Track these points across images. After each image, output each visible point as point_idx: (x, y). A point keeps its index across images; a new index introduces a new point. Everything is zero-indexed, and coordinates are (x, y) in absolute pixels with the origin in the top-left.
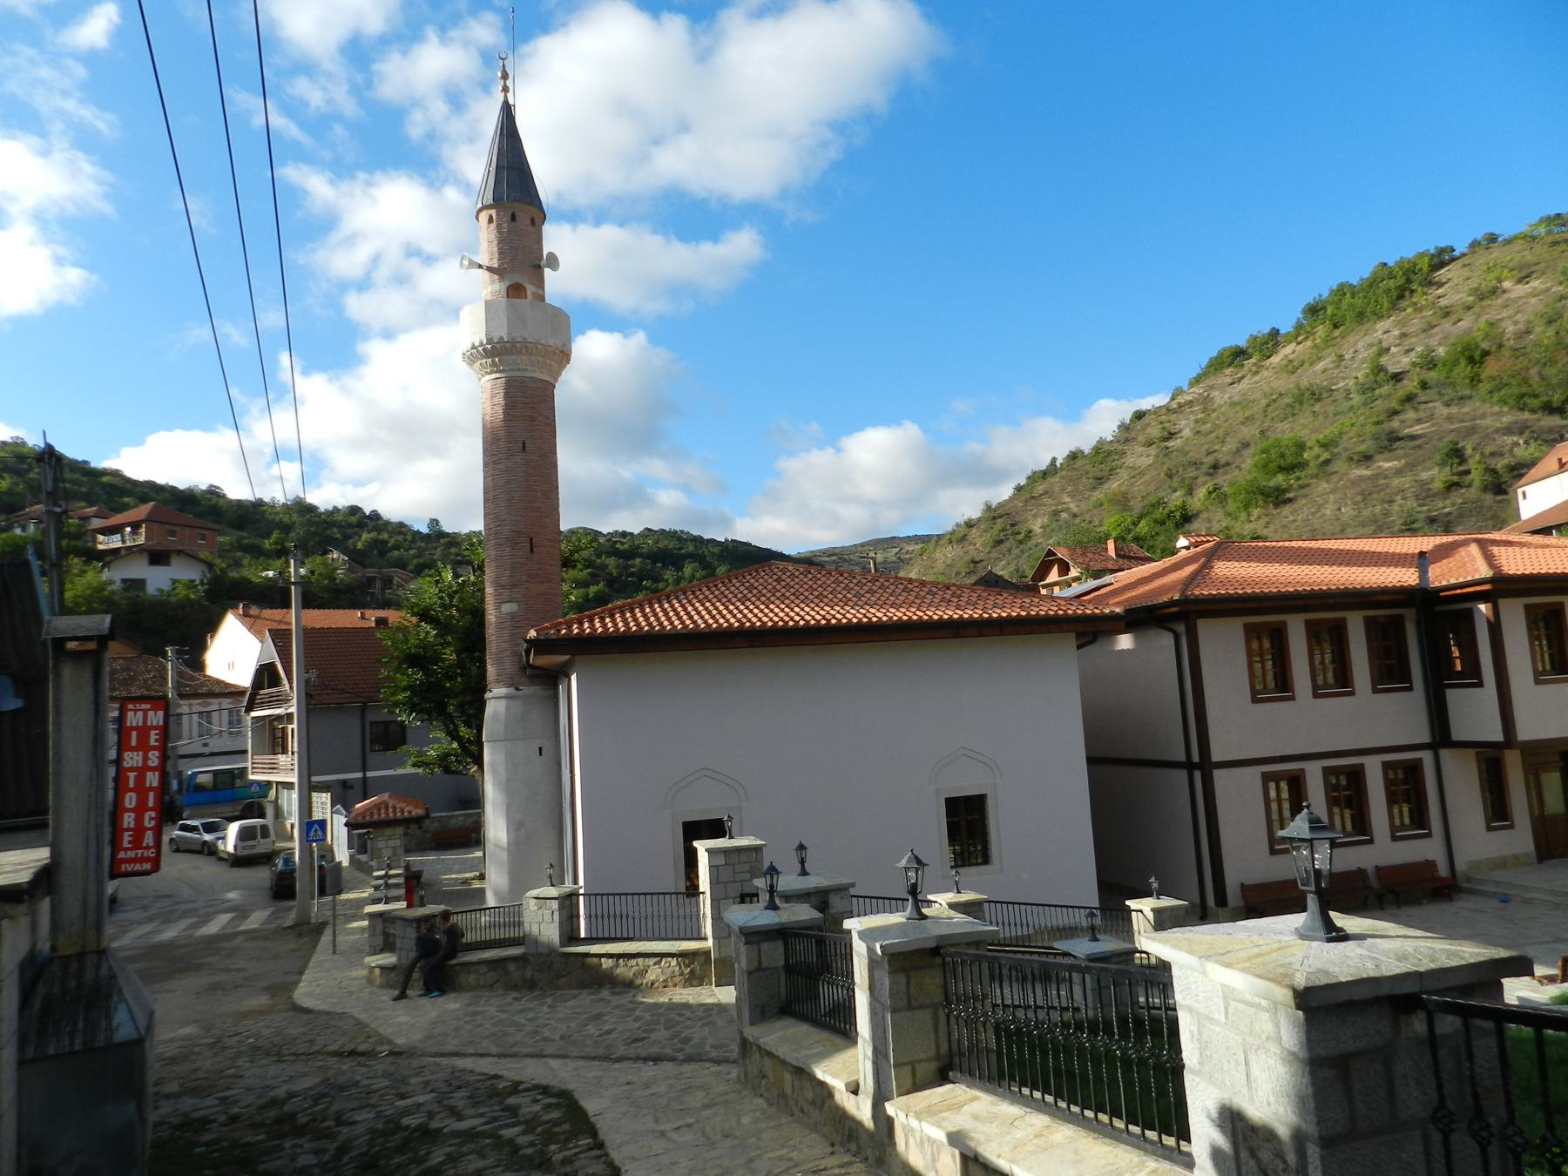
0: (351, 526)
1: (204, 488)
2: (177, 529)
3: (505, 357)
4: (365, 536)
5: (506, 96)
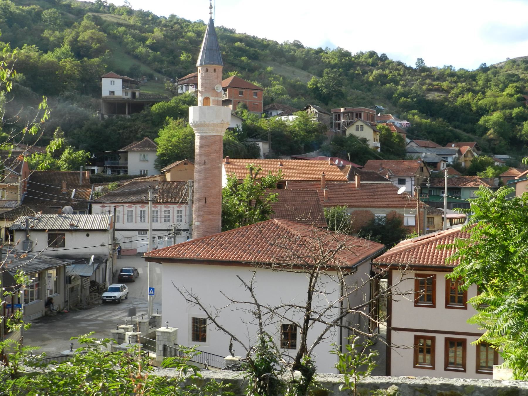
0: (368, 65)
1: (292, 42)
2: (244, 90)
3: (199, 128)
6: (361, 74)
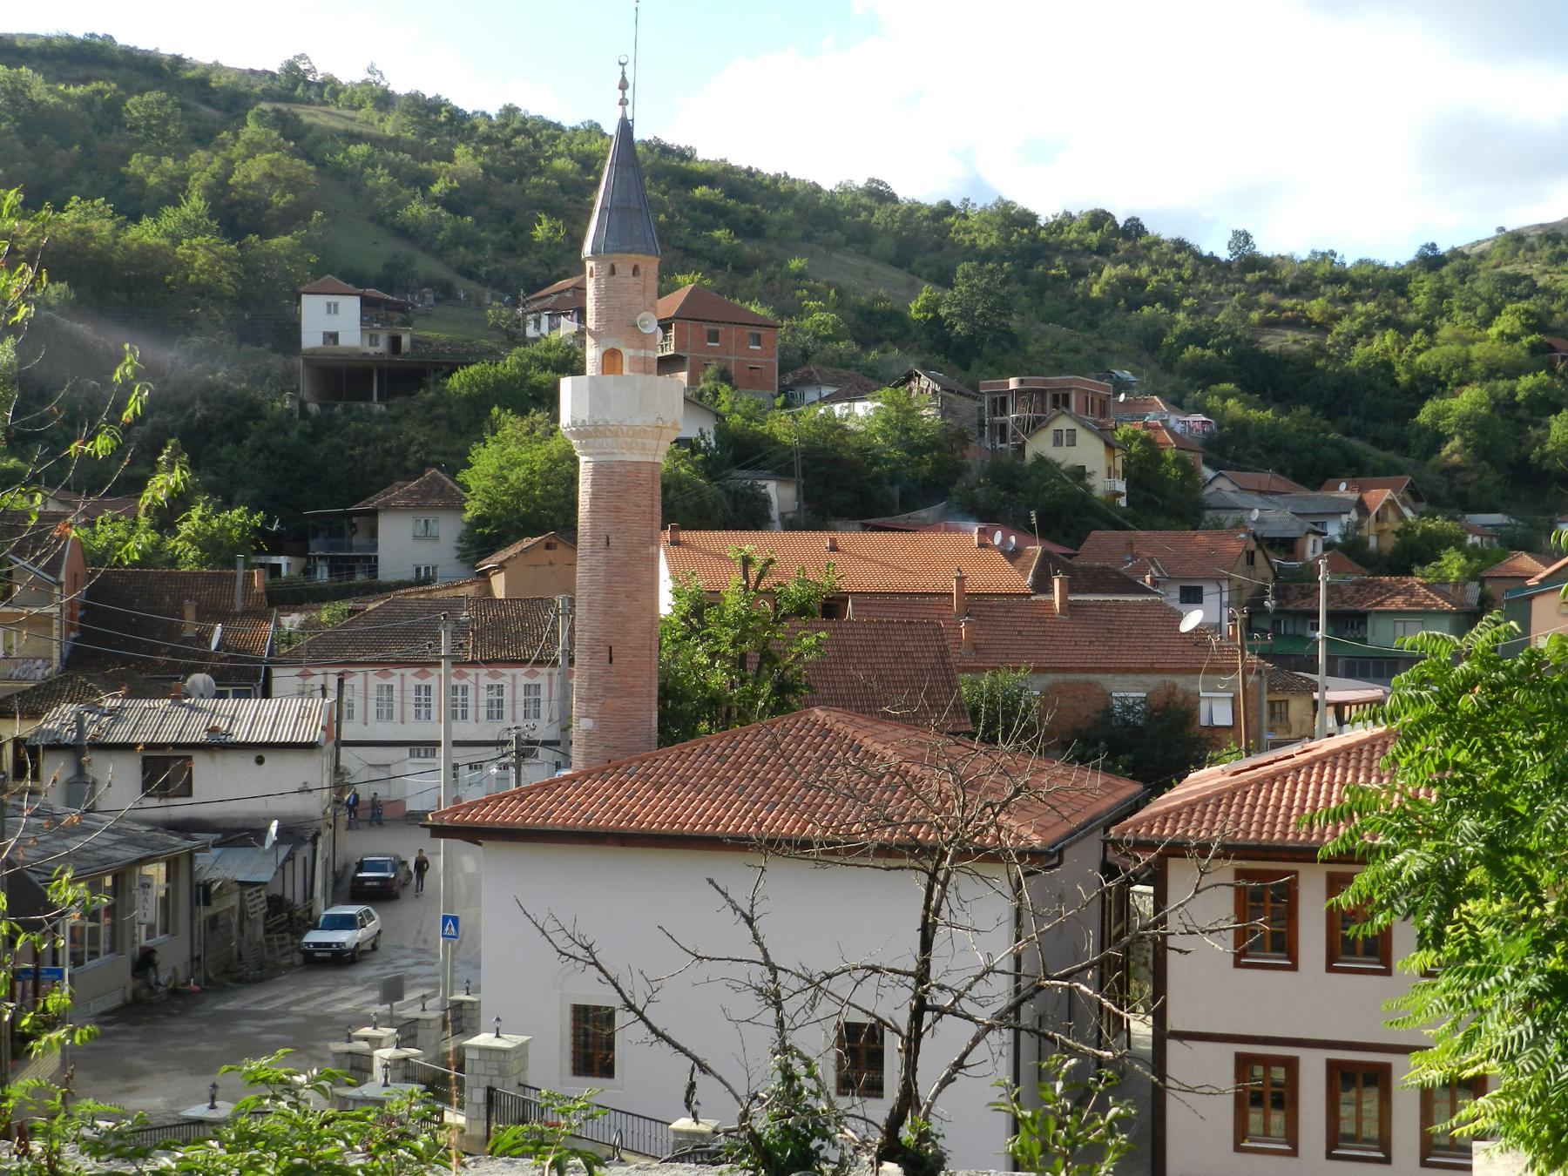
0: (1088, 250)
2: (721, 328)
4: (1109, 272)
5: (624, 110)
6: (1067, 276)
